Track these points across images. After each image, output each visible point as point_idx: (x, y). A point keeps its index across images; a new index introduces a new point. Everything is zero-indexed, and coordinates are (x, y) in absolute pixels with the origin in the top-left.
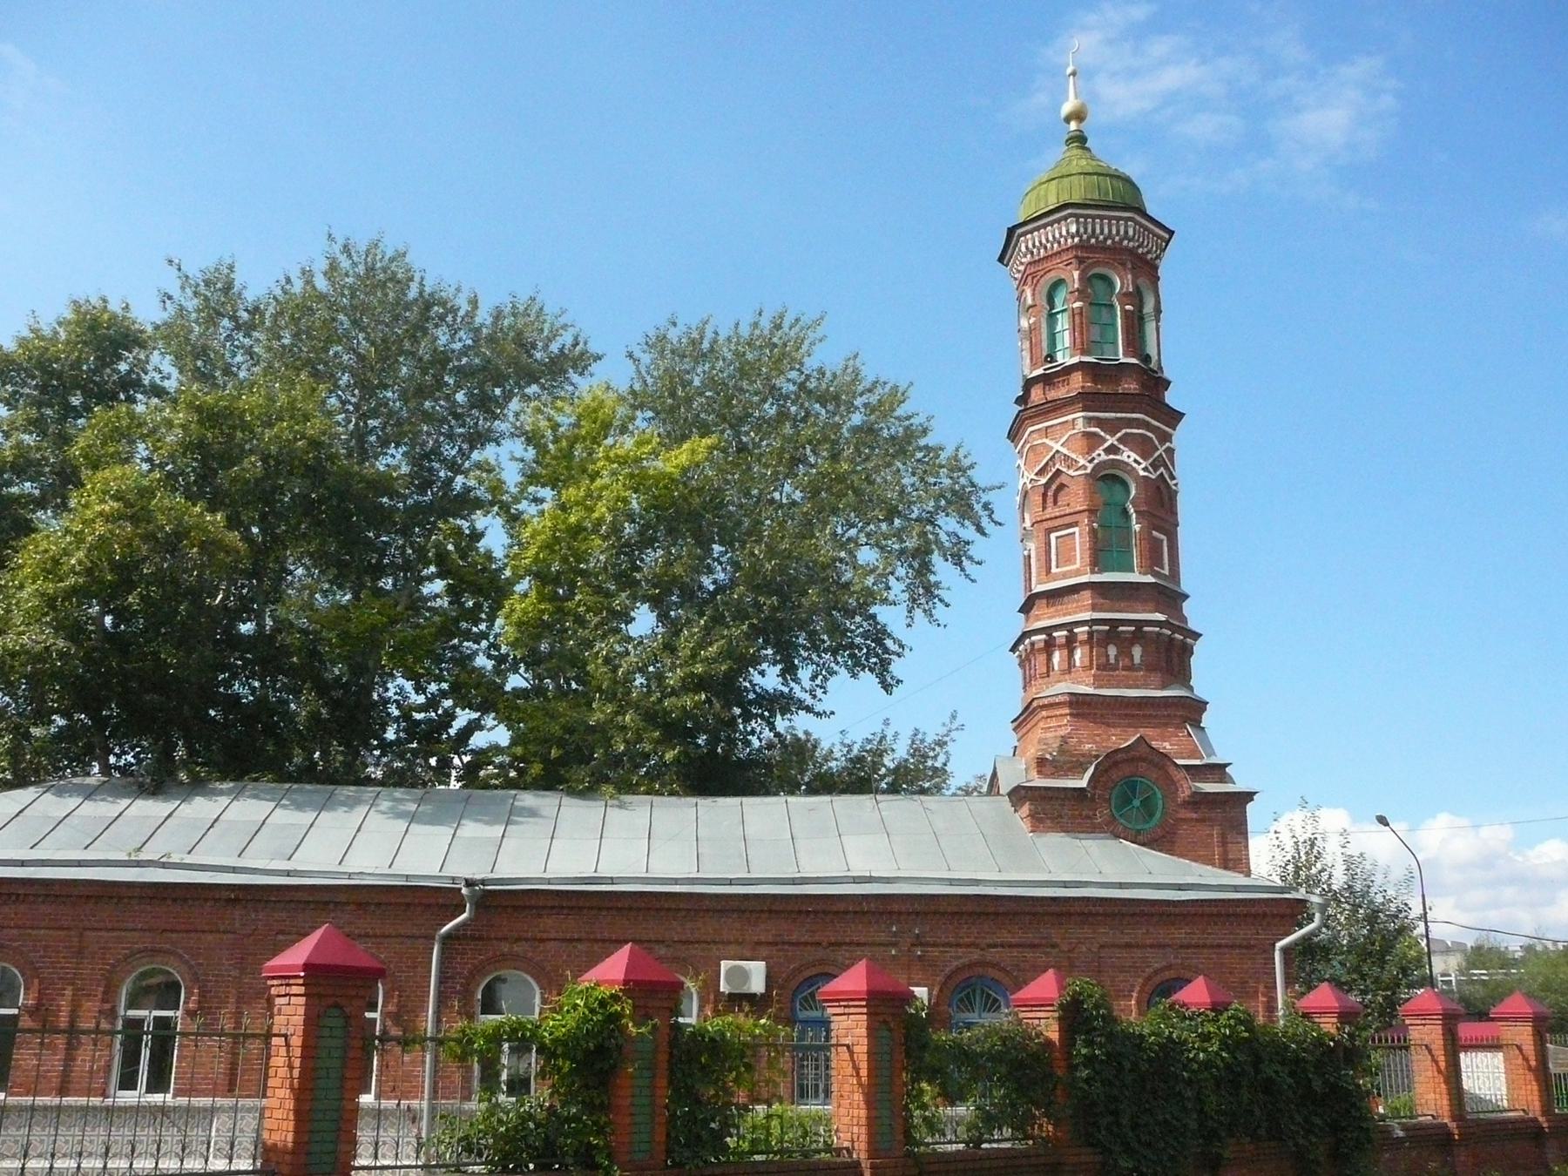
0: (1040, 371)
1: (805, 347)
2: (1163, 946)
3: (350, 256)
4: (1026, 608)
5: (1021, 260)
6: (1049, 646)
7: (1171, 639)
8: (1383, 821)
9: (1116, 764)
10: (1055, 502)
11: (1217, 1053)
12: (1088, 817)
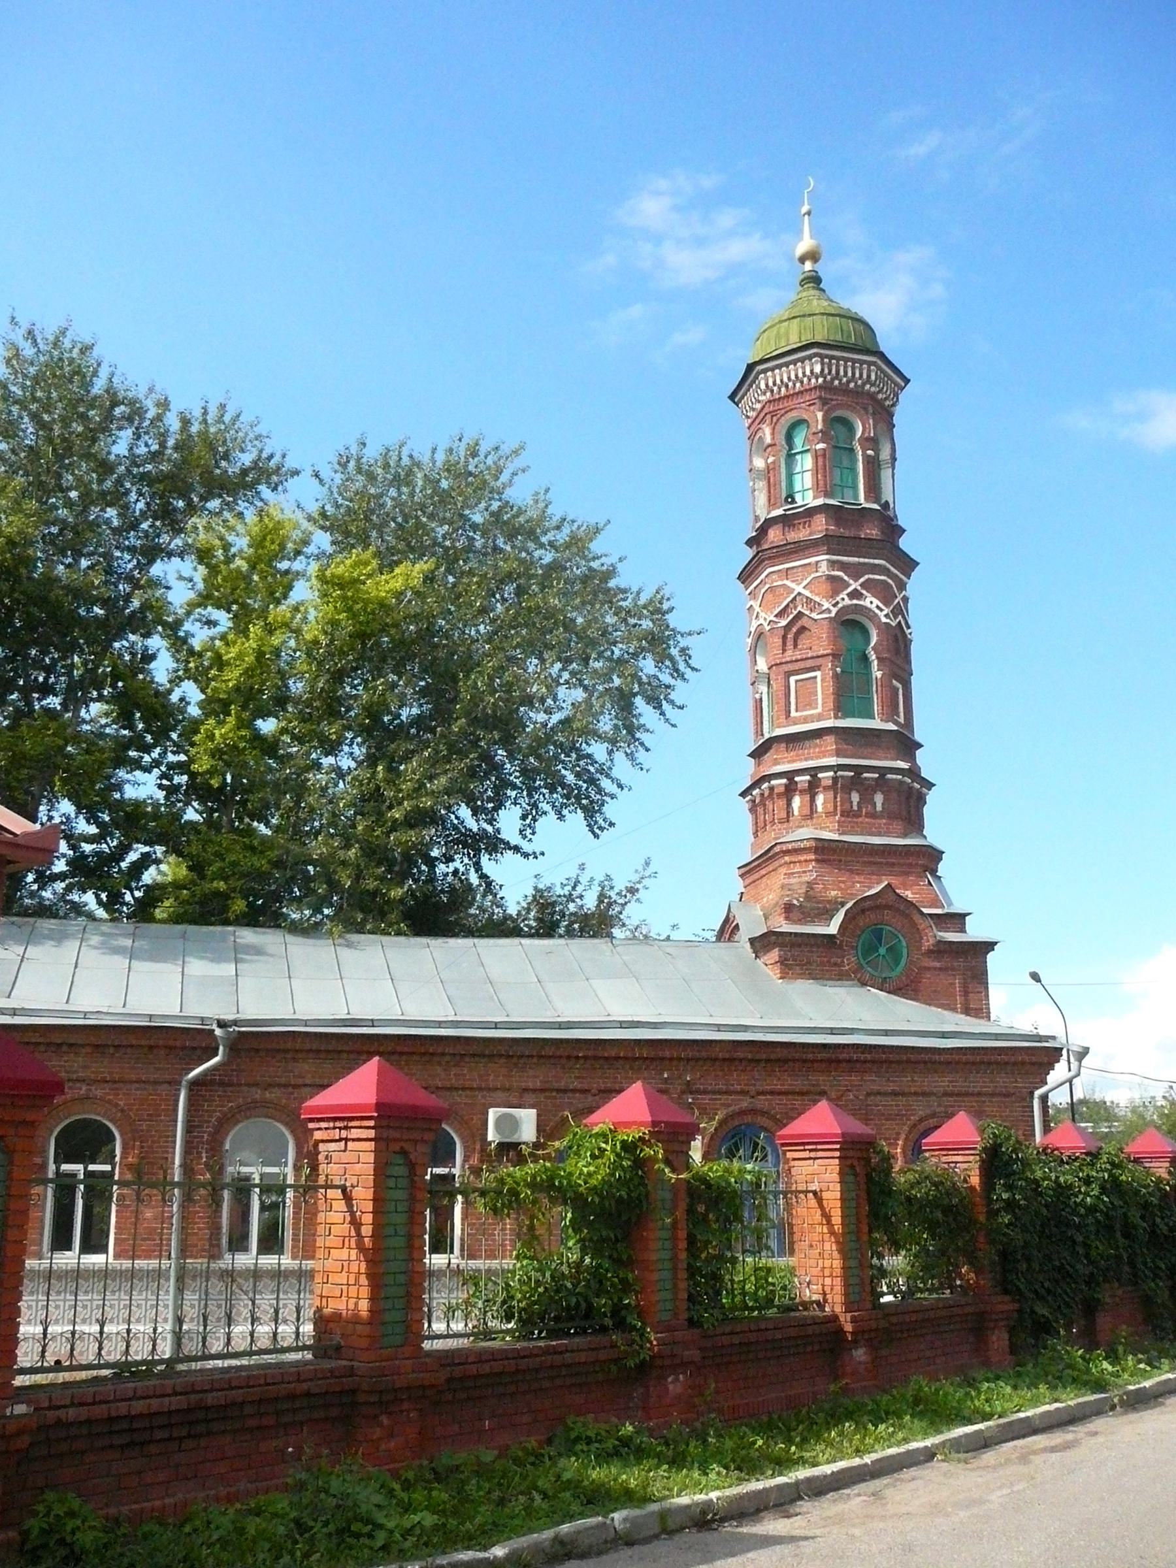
0: (779, 512)
1: (504, 478)
2: (924, 1094)
3: (35, 343)
4: (758, 754)
5: (756, 398)
6: (790, 790)
7: (911, 788)
8: (1035, 977)
9: (863, 911)
10: (795, 646)
11: (1098, 1198)
12: (835, 964)
